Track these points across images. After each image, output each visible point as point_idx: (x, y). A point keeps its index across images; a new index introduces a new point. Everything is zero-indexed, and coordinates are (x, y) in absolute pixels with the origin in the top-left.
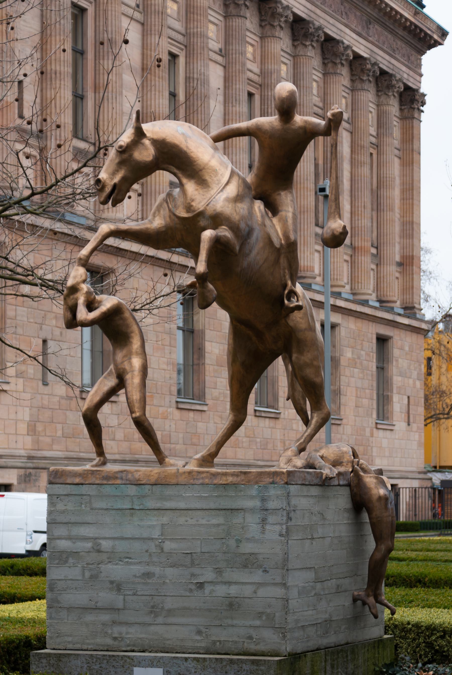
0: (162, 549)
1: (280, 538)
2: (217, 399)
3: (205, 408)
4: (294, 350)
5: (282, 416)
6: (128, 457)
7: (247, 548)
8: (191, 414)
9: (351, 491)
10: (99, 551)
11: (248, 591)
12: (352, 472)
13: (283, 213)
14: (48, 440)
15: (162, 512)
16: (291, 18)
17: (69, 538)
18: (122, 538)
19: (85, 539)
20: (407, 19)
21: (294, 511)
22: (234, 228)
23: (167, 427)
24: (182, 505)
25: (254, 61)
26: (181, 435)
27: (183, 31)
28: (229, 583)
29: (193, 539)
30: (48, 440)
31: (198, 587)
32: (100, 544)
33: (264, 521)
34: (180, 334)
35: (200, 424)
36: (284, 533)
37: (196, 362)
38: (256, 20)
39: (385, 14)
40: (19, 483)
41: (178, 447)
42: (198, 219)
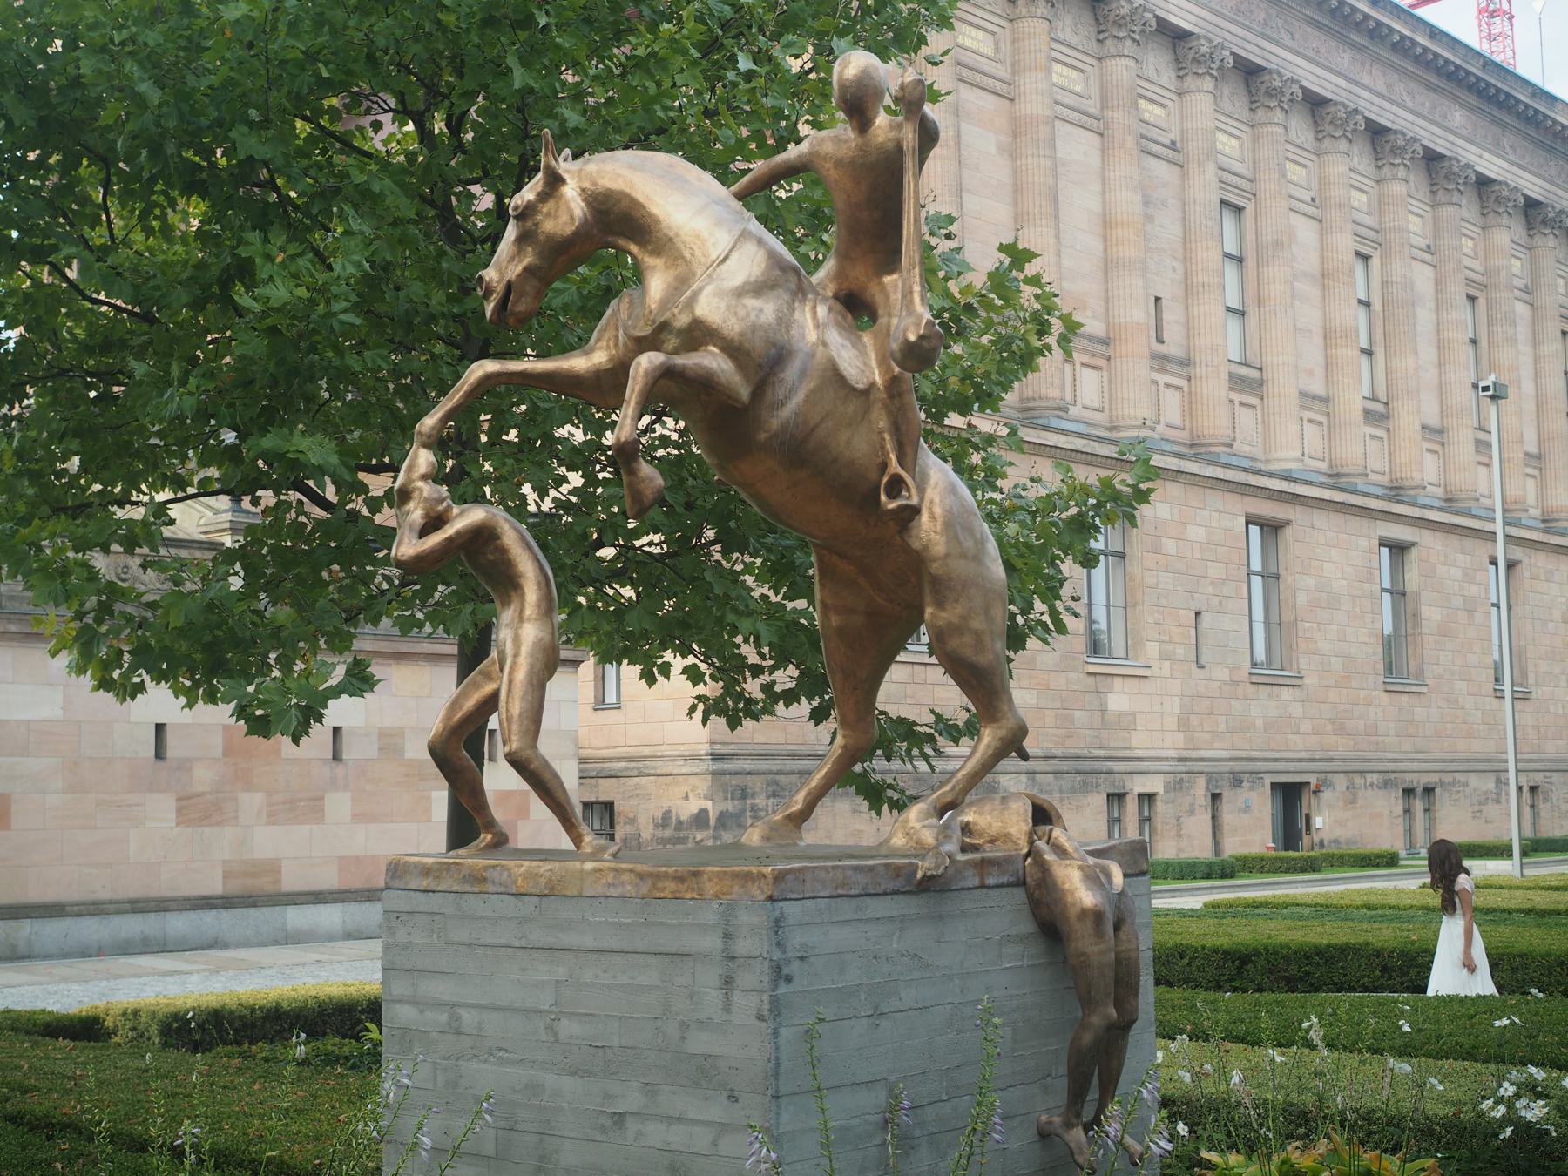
0: (555, 1034)
1: (757, 1023)
2: (1440, 677)
3: (1424, 689)
4: (928, 598)
5: (1534, 695)
6: (1317, 755)
7: (699, 1042)
8: (1405, 698)
9: (1030, 896)
10: (459, 1033)
11: (701, 1139)
12: (1028, 855)
13: (882, 321)
14: (1207, 736)
15: (558, 954)
16: (1522, 201)
17: (414, 1002)
18: (494, 1008)
19: (438, 1005)
20: (1447, 61)
21: (802, 958)
22: (733, 349)
23: (1372, 715)
24: (589, 941)
25: (1475, 257)
26: (1392, 725)
27: (1377, 227)
28: (670, 1120)
29: (607, 1016)
30: (1207, 736)
31: (615, 1124)
32: (459, 1018)
33: (728, 982)
34: (1387, 597)
35: (1417, 710)
36: (766, 1013)
37: (1410, 631)
38: (1475, 207)
39: (1556, 135)
40: (1166, 792)
41: (1388, 739)
42: (662, 336)
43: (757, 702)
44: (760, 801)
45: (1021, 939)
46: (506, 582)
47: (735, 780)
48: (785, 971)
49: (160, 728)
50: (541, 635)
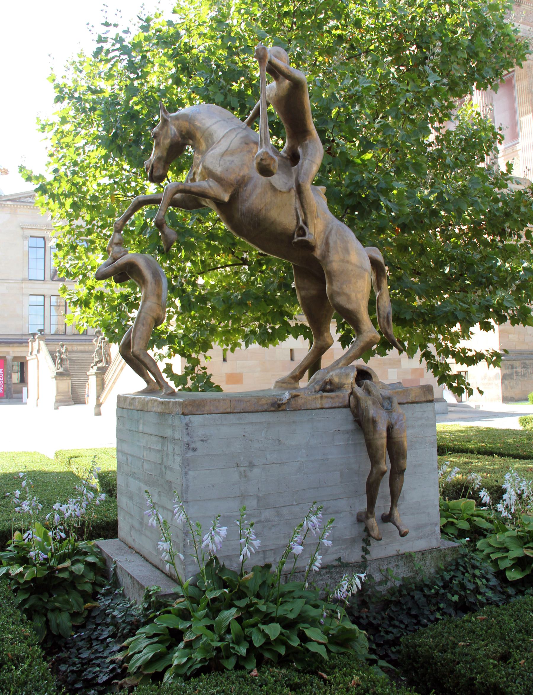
21: (202, 440)
43: (74, 201)
44: (519, 370)
45: (347, 432)
46: (283, 127)
47: (509, 363)
48: (192, 446)
49: (291, 350)
50: (247, 205)
